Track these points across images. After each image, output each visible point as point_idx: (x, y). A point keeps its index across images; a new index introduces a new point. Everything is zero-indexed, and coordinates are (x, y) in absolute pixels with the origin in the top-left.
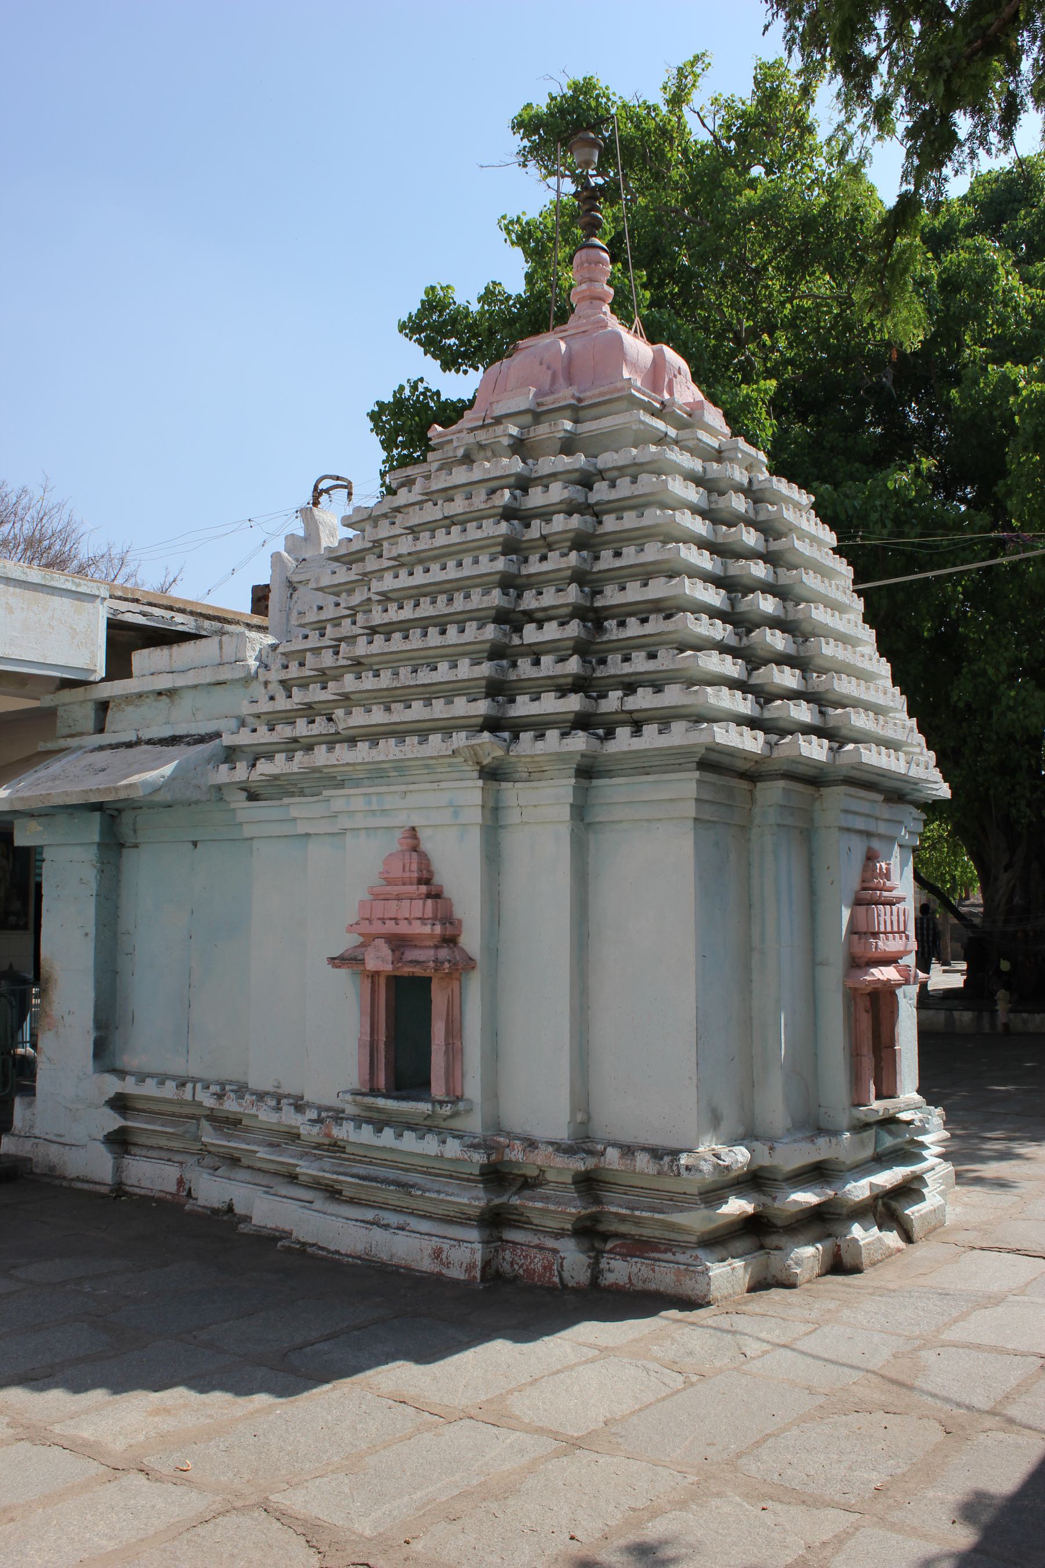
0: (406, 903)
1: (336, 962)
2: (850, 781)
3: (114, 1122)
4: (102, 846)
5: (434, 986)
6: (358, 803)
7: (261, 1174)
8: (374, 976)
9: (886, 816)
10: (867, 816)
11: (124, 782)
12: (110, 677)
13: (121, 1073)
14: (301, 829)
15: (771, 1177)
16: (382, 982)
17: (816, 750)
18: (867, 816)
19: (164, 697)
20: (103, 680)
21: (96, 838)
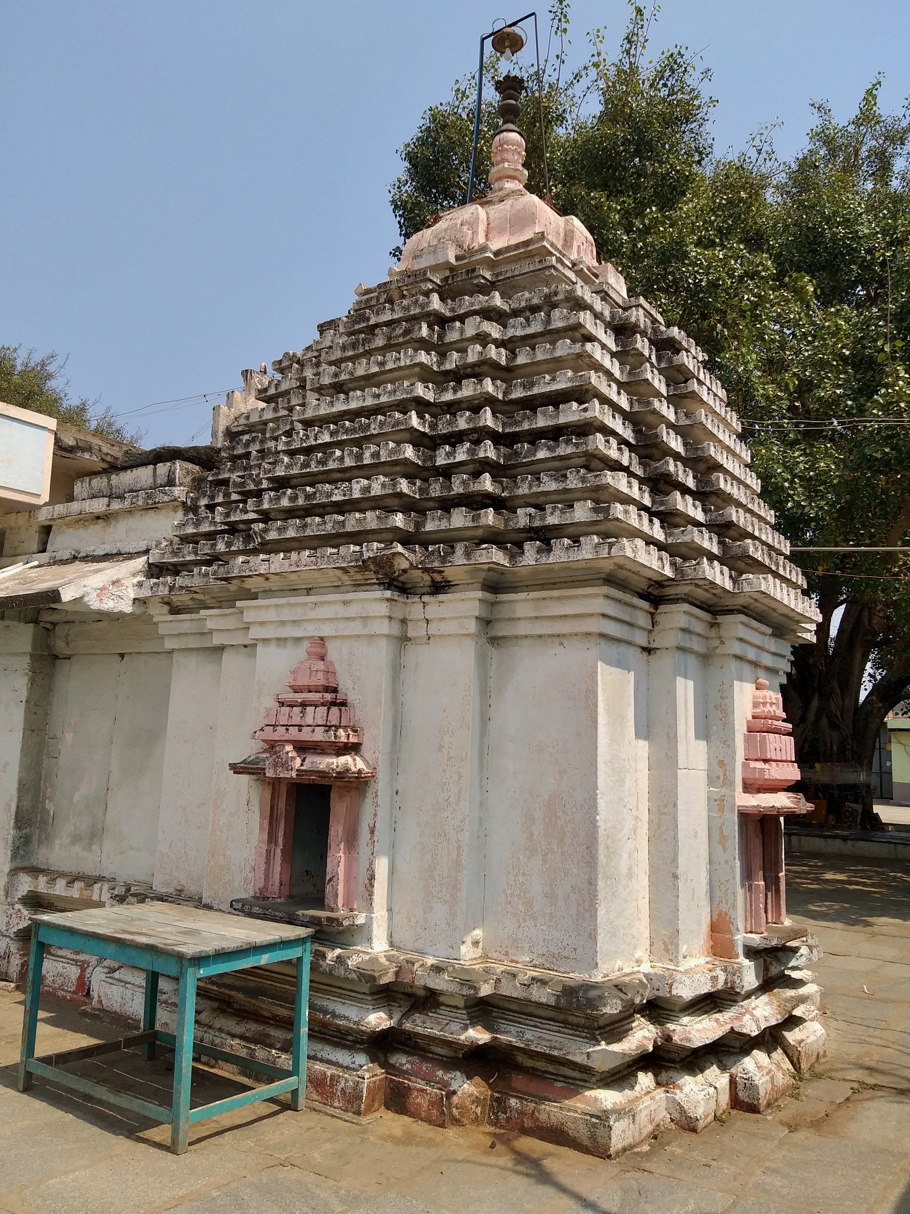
0: (310, 709)
1: (237, 769)
2: (744, 610)
3: (24, 918)
4: (34, 657)
5: (334, 796)
6: (271, 615)
7: (757, 634)
8: (275, 783)
9: (773, 650)
10: (759, 647)
11: (502, 1131)
12: (52, 502)
13: (35, 871)
14: (217, 640)
15: (668, 1007)
16: (283, 790)
17: (717, 575)
18: (759, 647)
19: (101, 521)
20: (46, 504)
21: (28, 648)
